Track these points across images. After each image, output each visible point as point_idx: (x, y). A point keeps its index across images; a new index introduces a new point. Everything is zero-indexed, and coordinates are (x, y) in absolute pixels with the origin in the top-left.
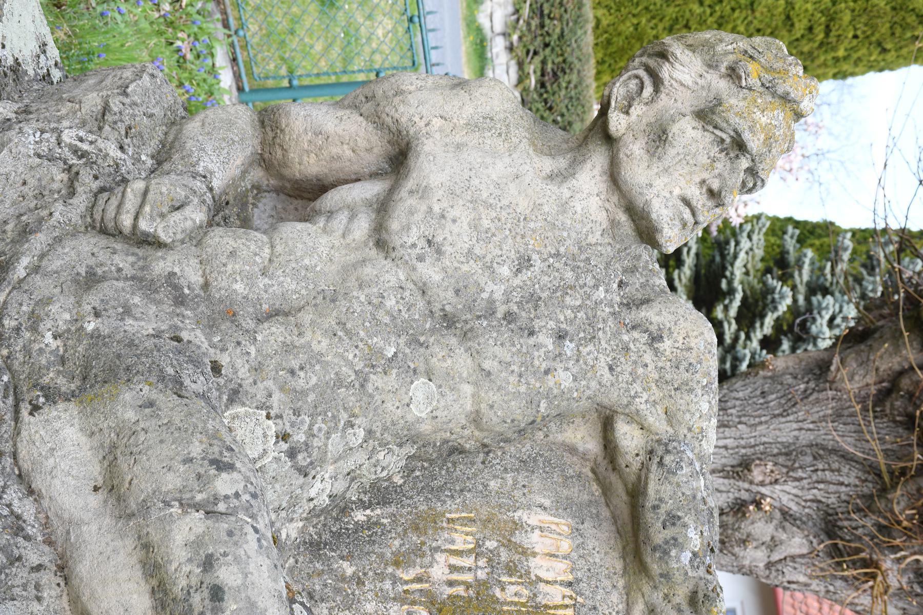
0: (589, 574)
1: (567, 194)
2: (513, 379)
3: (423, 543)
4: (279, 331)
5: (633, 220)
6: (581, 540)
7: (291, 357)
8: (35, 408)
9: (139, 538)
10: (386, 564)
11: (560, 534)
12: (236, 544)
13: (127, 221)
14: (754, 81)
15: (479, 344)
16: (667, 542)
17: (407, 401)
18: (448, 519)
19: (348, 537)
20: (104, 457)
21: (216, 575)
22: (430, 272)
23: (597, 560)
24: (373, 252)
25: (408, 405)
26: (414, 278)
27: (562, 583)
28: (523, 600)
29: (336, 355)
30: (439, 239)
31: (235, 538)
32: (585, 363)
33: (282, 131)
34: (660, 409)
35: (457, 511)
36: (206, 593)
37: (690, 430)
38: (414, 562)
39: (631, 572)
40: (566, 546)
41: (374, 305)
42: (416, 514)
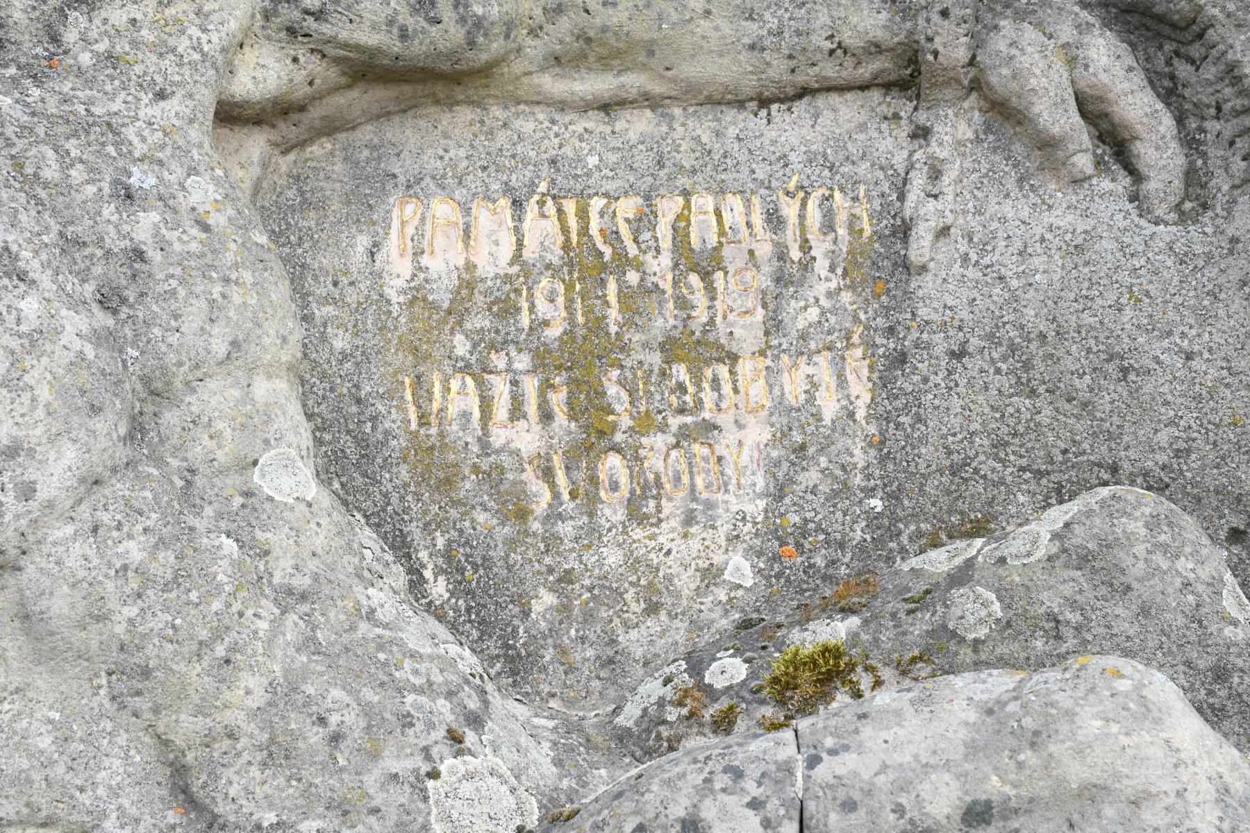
0: (492, 169)
3: (476, 469)
4: (235, 778)
6: (428, 180)
7: (301, 744)
10: (527, 533)
11: (423, 219)
12: (869, 793)
15: (180, 364)
16: (462, 20)
17: (303, 507)
18: (421, 425)
19: (484, 606)
21: (944, 822)
23: (462, 153)
25: (310, 505)
26: (70, 503)
28: (561, 288)
29: (268, 654)
31: (857, 796)
32: (162, 147)
35: (402, 409)
38: (514, 483)
39: (482, 92)
40: (442, 209)
42: (418, 484)
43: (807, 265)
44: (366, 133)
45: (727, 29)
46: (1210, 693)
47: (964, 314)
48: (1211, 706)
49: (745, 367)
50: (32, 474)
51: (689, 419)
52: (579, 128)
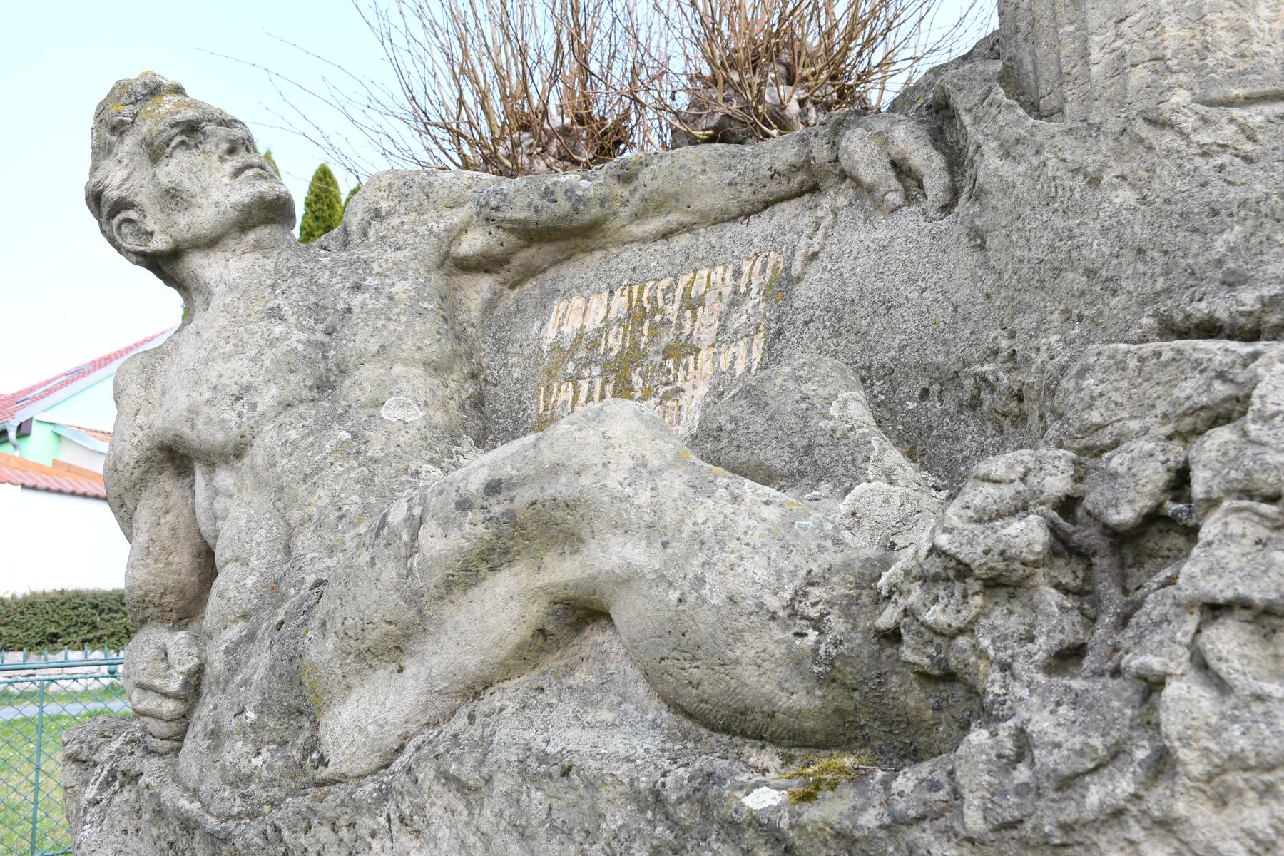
1: (222, 287)
2: (391, 326)
5: (254, 226)
8: (323, 762)
9: (441, 598)
13: (170, 707)
14: (127, 110)
17: (401, 425)
20: (370, 667)
22: (267, 398)
24: (246, 460)
26: (273, 414)
27: (610, 299)
28: (622, 330)
30: (235, 389)
33: (146, 595)
34: (449, 212)
35: (537, 403)
36: (492, 500)
37: (468, 187)
39: (604, 241)
41: (294, 450)
43: (746, 295)
44: (552, 273)
45: (715, 177)
46: (801, 462)
47: (816, 300)
48: (799, 471)
49: (703, 355)
50: (256, 399)
51: (669, 388)
52: (652, 250)
